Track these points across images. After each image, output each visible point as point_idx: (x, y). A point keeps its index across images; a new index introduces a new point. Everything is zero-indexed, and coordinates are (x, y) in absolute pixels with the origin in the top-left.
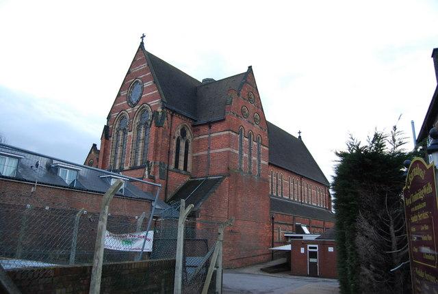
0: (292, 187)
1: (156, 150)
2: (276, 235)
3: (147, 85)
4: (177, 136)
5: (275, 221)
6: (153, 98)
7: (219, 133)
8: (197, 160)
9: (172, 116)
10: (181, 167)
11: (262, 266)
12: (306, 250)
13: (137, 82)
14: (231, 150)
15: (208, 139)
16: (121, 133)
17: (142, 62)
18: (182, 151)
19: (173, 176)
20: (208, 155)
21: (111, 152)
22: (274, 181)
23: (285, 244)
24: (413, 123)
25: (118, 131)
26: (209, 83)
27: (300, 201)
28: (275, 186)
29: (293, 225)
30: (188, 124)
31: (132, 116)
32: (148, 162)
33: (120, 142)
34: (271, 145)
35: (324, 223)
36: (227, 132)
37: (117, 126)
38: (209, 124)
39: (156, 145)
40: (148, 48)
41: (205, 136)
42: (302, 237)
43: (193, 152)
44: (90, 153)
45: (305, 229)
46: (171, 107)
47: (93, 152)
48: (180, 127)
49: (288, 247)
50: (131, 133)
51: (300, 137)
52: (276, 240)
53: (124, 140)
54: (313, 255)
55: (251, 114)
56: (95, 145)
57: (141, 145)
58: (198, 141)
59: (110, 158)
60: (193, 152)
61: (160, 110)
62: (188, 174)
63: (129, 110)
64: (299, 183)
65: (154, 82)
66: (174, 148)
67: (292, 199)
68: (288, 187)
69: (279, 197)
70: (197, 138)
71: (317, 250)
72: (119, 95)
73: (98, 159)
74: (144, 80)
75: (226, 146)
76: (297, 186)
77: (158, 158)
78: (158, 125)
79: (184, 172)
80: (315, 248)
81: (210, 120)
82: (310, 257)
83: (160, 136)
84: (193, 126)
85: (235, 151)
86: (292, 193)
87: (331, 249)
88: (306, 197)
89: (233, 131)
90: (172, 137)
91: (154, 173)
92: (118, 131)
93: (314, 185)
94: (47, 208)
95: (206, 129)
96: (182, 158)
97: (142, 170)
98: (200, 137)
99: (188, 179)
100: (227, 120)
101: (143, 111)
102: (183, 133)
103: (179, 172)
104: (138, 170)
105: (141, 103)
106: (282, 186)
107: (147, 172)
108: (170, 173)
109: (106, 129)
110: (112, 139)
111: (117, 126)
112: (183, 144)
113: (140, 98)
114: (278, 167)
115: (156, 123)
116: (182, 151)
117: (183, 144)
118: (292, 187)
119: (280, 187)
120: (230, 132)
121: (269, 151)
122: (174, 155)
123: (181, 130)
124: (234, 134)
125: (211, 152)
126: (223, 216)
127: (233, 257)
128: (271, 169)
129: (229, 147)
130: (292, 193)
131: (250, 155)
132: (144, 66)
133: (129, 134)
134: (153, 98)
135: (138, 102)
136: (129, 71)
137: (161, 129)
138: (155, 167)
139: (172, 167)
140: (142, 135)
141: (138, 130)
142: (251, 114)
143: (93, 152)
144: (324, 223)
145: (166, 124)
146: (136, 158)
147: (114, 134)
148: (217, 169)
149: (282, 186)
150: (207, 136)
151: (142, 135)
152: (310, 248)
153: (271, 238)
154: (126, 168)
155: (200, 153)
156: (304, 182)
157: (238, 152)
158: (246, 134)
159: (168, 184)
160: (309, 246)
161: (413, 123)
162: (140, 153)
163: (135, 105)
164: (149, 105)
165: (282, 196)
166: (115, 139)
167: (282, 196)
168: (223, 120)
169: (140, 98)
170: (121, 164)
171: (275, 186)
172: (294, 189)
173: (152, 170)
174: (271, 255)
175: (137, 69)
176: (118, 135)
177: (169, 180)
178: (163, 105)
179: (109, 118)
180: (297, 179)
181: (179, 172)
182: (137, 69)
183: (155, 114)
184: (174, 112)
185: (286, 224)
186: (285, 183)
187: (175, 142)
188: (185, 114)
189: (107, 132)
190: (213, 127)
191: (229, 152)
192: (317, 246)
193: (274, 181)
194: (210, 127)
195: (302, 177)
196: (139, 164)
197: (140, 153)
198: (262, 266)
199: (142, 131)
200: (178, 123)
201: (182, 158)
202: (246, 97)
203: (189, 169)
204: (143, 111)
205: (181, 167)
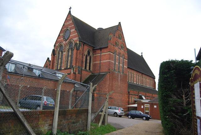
2: (130, 100)
3: (72, 30)
4: (86, 54)
6: (75, 37)
7: (105, 53)
8: (95, 65)
10: (88, 68)
12: (144, 107)
13: (68, 29)
14: (110, 61)
15: (100, 56)
16: (60, 53)
17: (70, 20)
18: (88, 61)
20: (100, 63)
21: (56, 62)
23: (134, 104)
24: (195, 49)
25: (59, 52)
26: (100, 30)
27: (141, 84)
28: (130, 78)
29: (138, 95)
31: (66, 45)
33: (60, 57)
34: (129, 59)
38: (101, 49)
39: (76, 58)
40: (73, 14)
41: (99, 55)
42: (140, 101)
43: (93, 62)
45: (144, 97)
46: (83, 41)
47: (47, 62)
48: (87, 50)
50: (65, 53)
51: (142, 55)
52: (130, 102)
53: (62, 56)
55: (120, 45)
56: (48, 58)
57: (69, 58)
59: (55, 64)
60: (93, 62)
61: (78, 42)
62: (91, 72)
63: (64, 42)
65: (76, 30)
66: (84, 59)
68: (136, 78)
69: (138, 84)
70: (95, 55)
72: (59, 35)
73: (50, 65)
74: (71, 28)
75: (108, 59)
77: (77, 64)
78: (77, 50)
79: (89, 71)
83: (78, 54)
85: (112, 61)
86: (138, 81)
87: (155, 107)
90: (84, 55)
91: (76, 71)
92: (59, 52)
93: (148, 78)
94: (28, 86)
95: (99, 51)
96: (88, 64)
98: (96, 55)
99: (91, 74)
101: (70, 43)
102: (89, 53)
105: (69, 39)
107: (72, 71)
108: (83, 71)
109: (54, 51)
110: (56, 55)
112: (88, 58)
114: (132, 69)
115: (76, 48)
116: (88, 61)
117: (88, 58)
119: (132, 78)
122: (84, 63)
124: (112, 54)
126: (106, 91)
130: (138, 81)
131: (119, 63)
132: (71, 22)
134: (75, 37)
135: (68, 38)
137: (79, 51)
138: (76, 68)
139: (84, 68)
140: (70, 54)
141: (68, 51)
142: (120, 45)
145: (81, 49)
146: (67, 64)
147: (57, 53)
148: (104, 69)
151: (70, 54)
152: (146, 106)
154: (63, 69)
156: (143, 76)
157: (113, 62)
158: (117, 54)
160: (145, 105)
161: (195, 49)
163: (66, 40)
164: (73, 40)
165: (133, 82)
166: (58, 55)
167: (133, 82)
168: (107, 47)
170: (61, 67)
171: (130, 78)
173: (75, 69)
174: (128, 109)
175: (68, 23)
176: (59, 54)
178: (80, 40)
179: (55, 46)
180: (141, 75)
181: (87, 71)
182: (68, 23)
183: (76, 44)
184: (84, 43)
185: (135, 95)
186: (135, 77)
187: (85, 57)
188: (90, 44)
190: (102, 50)
191: (110, 62)
192: (149, 105)
194: (101, 50)
195: (142, 74)
196: (69, 67)
199: (70, 52)
200: (86, 49)
201: (88, 64)
203: (91, 69)
204: (70, 43)
205: (88, 68)
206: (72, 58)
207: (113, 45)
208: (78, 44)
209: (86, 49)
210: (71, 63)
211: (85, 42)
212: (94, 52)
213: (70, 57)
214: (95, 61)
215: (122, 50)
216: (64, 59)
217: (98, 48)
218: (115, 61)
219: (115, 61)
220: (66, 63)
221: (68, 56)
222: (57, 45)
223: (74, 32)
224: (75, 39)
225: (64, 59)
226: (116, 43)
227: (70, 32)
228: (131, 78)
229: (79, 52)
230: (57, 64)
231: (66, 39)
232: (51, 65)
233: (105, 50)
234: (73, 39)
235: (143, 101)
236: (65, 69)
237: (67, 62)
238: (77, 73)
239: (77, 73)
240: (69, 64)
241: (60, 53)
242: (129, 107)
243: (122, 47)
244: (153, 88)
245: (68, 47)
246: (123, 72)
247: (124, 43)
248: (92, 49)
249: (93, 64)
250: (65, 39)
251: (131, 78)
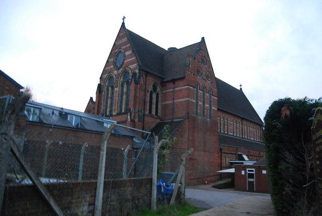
0: (235, 126)
1: (135, 100)
2: (224, 161)
3: (128, 53)
4: (150, 90)
5: (223, 151)
6: (132, 63)
9: (146, 76)
10: (154, 112)
11: (213, 184)
12: (246, 173)
13: (120, 51)
14: (189, 99)
15: (173, 92)
16: (110, 89)
17: (123, 37)
18: (154, 101)
19: (147, 119)
20: (173, 104)
21: (103, 103)
22: (222, 122)
23: (230, 168)
25: (108, 88)
26: (172, 50)
27: (241, 136)
28: (222, 125)
29: (236, 155)
30: (159, 82)
31: (118, 76)
32: (130, 109)
33: (109, 95)
35: (260, 153)
36: (187, 87)
37: (107, 84)
39: (135, 97)
40: (128, 27)
42: (243, 163)
44: (89, 103)
45: (245, 157)
48: (152, 83)
49: (232, 170)
51: (241, 89)
52: (224, 165)
53: (112, 93)
54: (251, 176)
55: (204, 73)
56: (91, 98)
57: (124, 97)
58: (166, 93)
59: (103, 108)
61: (137, 71)
63: (115, 72)
64: (241, 123)
67: (226, 133)
68: (232, 127)
70: (165, 91)
71: (254, 172)
73: (94, 108)
74: (126, 50)
75: (186, 97)
76: (239, 126)
78: (136, 83)
79: (155, 116)
80: (253, 171)
81: (174, 78)
82: (253, 174)
83: (138, 91)
84: (162, 83)
85: (192, 100)
86: (235, 131)
88: (246, 134)
89: (190, 86)
90: (147, 91)
91: (134, 117)
92: (108, 88)
95: (171, 85)
96: (154, 106)
97: (126, 115)
100: (187, 78)
101: (125, 73)
103: (152, 116)
104: (123, 116)
105: (124, 66)
106: (228, 125)
107: (129, 117)
109: (99, 86)
111: (107, 84)
112: (154, 96)
113: (123, 63)
115: (135, 81)
116: (154, 101)
117: (154, 96)
118: (235, 126)
119: (226, 127)
120: (189, 87)
121: (218, 100)
122: (148, 104)
123: (153, 86)
124: (192, 88)
125: (175, 101)
127: (192, 177)
128: (222, 115)
129: (188, 97)
130: (235, 131)
133: (116, 89)
134: (132, 63)
135: (121, 66)
136: (114, 44)
137: (139, 85)
138: (135, 113)
139: (147, 112)
140: (125, 90)
141: (122, 86)
143: (90, 103)
144: (260, 153)
145: (142, 82)
146: (121, 106)
147: (105, 89)
149: (228, 125)
150: (172, 90)
151: (125, 90)
152: (249, 171)
153: (220, 164)
155: (167, 102)
156: (244, 122)
157: (195, 101)
159: (145, 125)
160: (248, 169)
162: (124, 103)
163: (119, 69)
164: (130, 68)
165: (228, 132)
166: (106, 93)
167: (228, 132)
168: (184, 78)
169: (123, 63)
170: (111, 111)
171: (222, 125)
172: (237, 128)
173: (133, 115)
175: (120, 42)
177: (145, 122)
179: (101, 78)
181: (152, 116)
183: (134, 74)
184: (147, 73)
186: (231, 124)
187: (148, 94)
188: (156, 74)
189: (100, 88)
190: (176, 83)
191: (188, 101)
192: (254, 169)
193: (222, 122)
195: (243, 119)
196: (123, 111)
197: (124, 103)
198: (213, 184)
200: (151, 81)
201: (154, 106)
202: (200, 60)
203: (159, 114)
204: (125, 73)
205: (154, 112)
206: (128, 96)
207: (194, 74)
208: (137, 74)
209: (151, 81)
210: (127, 104)
211: (147, 70)
212: (162, 86)
213: (124, 95)
214: (165, 101)
215: (208, 81)
216: (116, 98)
217: (170, 78)
218: (197, 100)
219: (197, 100)
220: (119, 104)
221: (122, 93)
222: (105, 76)
223: (130, 55)
224: (132, 67)
225: (116, 98)
226: (198, 71)
227: (125, 56)
228: (224, 126)
229: (139, 87)
230: (104, 107)
231: (119, 66)
232: (96, 108)
233: (181, 83)
234: (130, 67)
235: (246, 163)
236: (118, 114)
237: (121, 103)
238: (136, 120)
239: (136, 120)
240: (124, 107)
241: (110, 89)
242: (221, 173)
243: (207, 77)
244: (243, 138)
245: (121, 80)
246: (211, 117)
247: (211, 69)
248: (159, 82)
249: (162, 105)
250: (117, 67)
251: (224, 126)
